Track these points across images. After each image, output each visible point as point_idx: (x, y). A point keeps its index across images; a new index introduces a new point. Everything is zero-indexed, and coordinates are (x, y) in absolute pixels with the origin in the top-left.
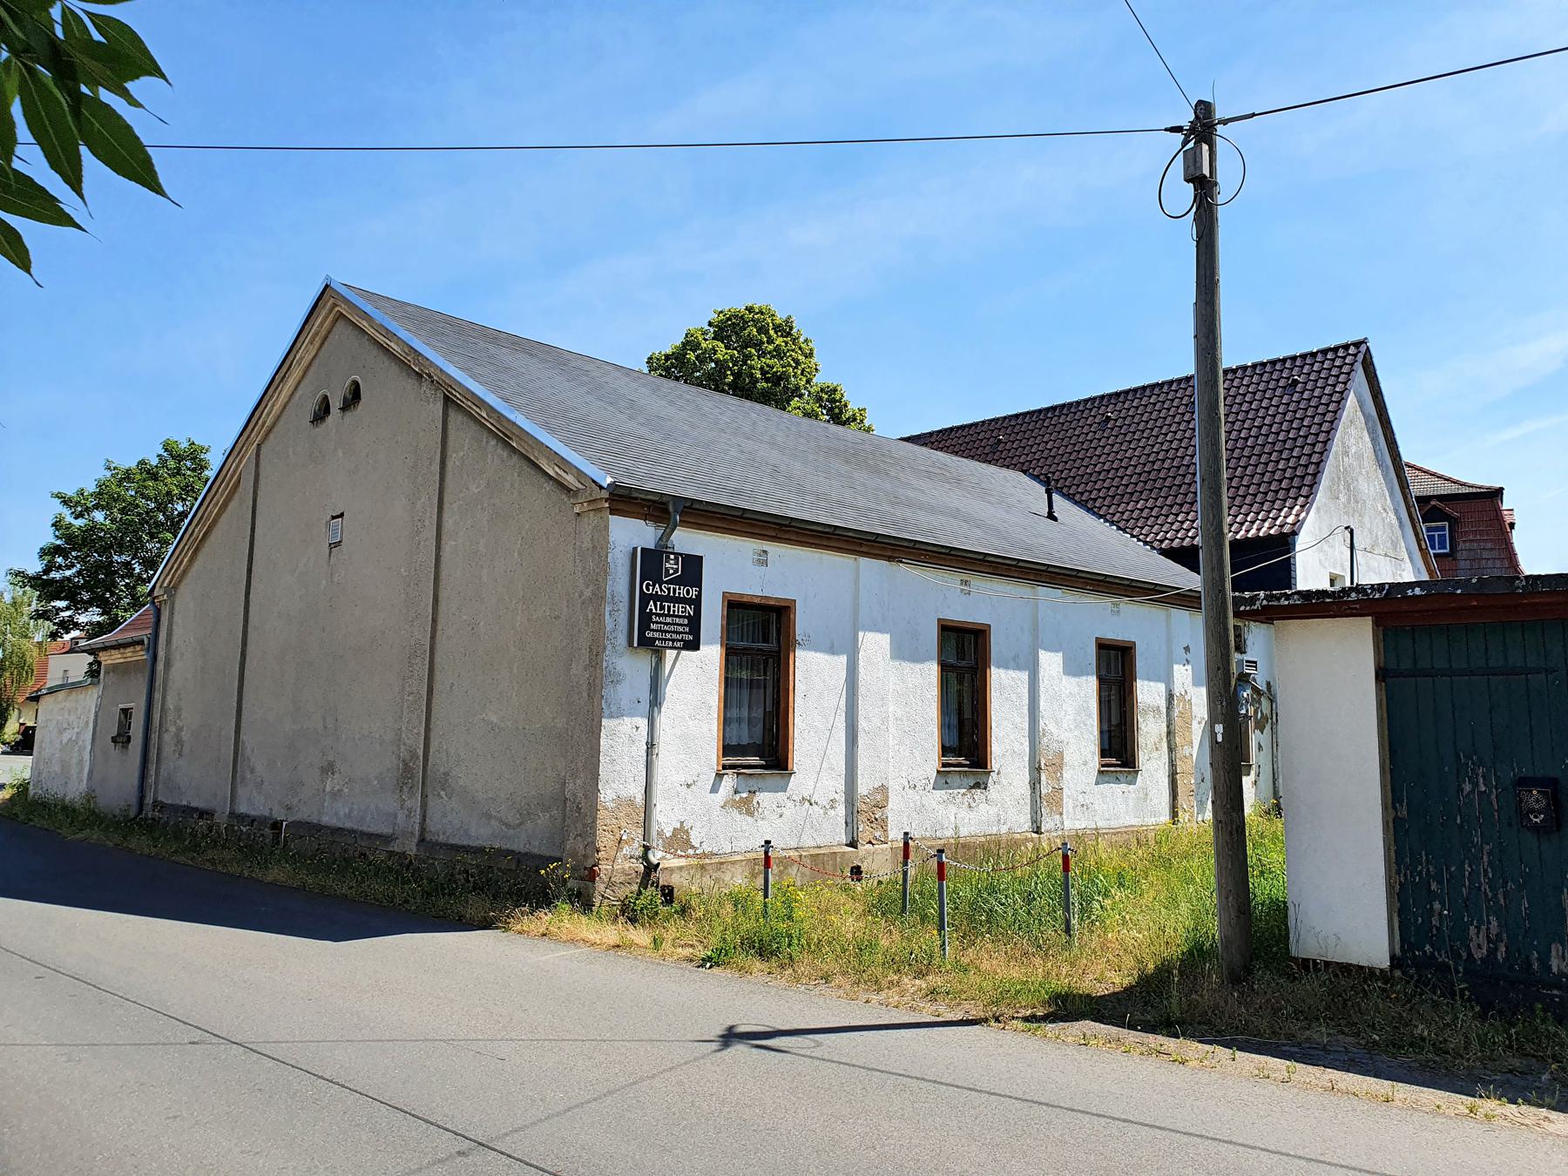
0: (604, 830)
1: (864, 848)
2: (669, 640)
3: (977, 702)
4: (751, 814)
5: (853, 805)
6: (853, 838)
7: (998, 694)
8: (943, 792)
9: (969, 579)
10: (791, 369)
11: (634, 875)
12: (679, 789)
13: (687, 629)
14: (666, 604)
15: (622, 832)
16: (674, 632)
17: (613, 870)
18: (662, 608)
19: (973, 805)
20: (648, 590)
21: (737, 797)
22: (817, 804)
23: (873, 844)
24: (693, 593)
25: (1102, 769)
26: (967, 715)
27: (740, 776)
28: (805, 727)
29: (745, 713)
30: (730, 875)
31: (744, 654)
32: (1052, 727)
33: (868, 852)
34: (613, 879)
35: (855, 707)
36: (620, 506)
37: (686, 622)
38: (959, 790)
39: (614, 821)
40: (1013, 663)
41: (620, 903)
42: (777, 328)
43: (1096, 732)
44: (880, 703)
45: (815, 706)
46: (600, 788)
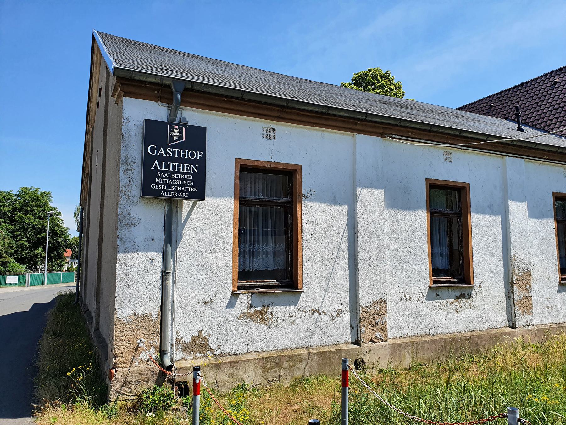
0: (121, 340)
1: (365, 346)
2: (174, 191)
3: (462, 237)
4: (266, 323)
5: (357, 313)
6: (357, 337)
7: (478, 232)
8: (435, 302)
9: (450, 151)
10: (388, 93)
11: (150, 374)
12: (198, 306)
13: (192, 183)
14: (171, 164)
15: (139, 341)
16: (179, 185)
17: (129, 372)
18: (167, 166)
19: (460, 310)
20: (153, 152)
21: (252, 310)
22: (325, 313)
23: (374, 342)
24: (198, 155)
25: (562, 281)
26: (456, 247)
27: (254, 295)
28: (313, 257)
29: (270, 248)
30: (244, 371)
31: (261, 205)
32: (521, 254)
33: (370, 349)
34: (128, 379)
35: (356, 242)
36: (130, 89)
37: (191, 177)
38: (447, 300)
39: (131, 333)
40: (490, 210)
41: (136, 397)
42: (382, 77)
43: (556, 256)
44: (377, 239)
45: (321, 241)
46: (116, 306)
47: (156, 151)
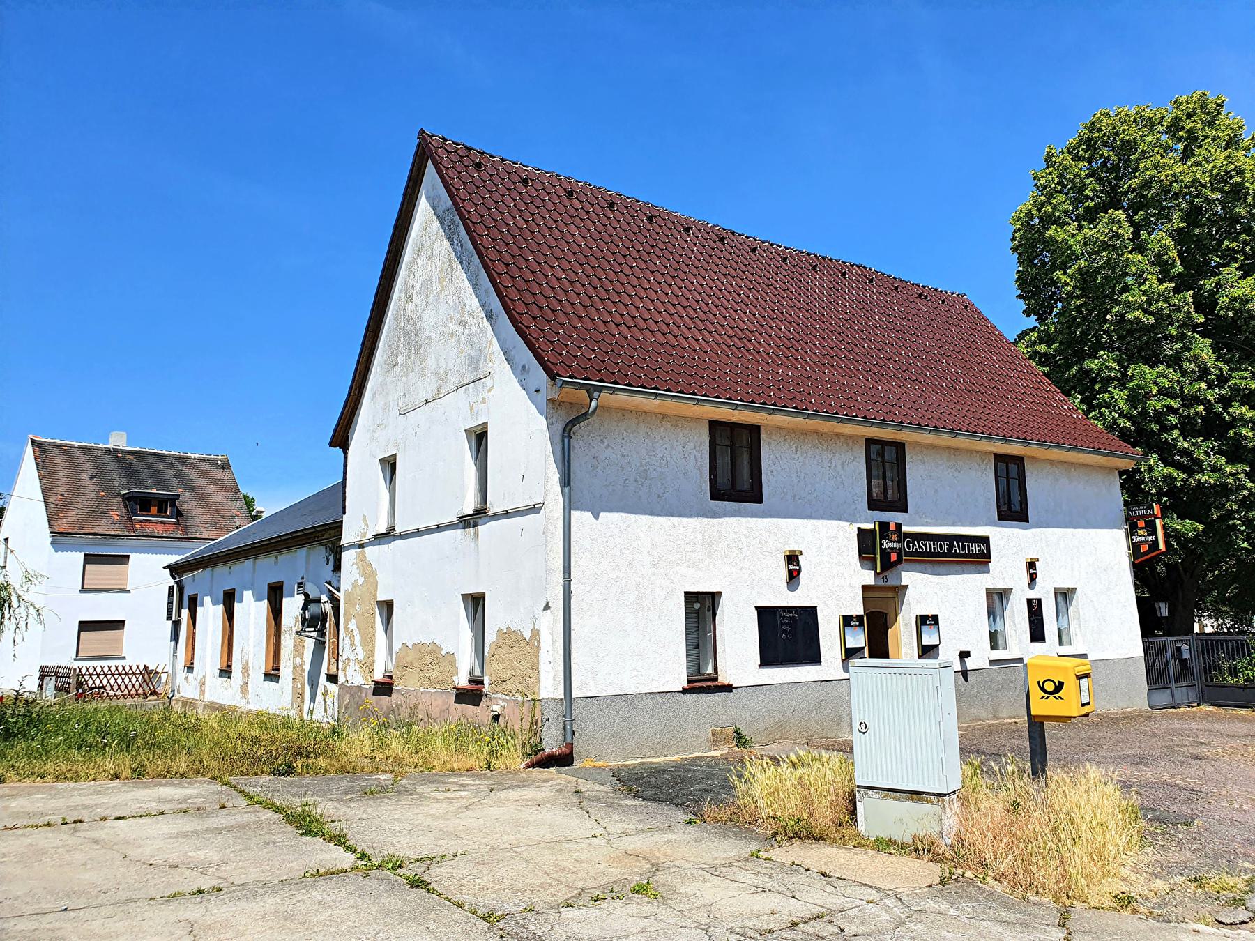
18: (964, 548)
20: (909, 548)
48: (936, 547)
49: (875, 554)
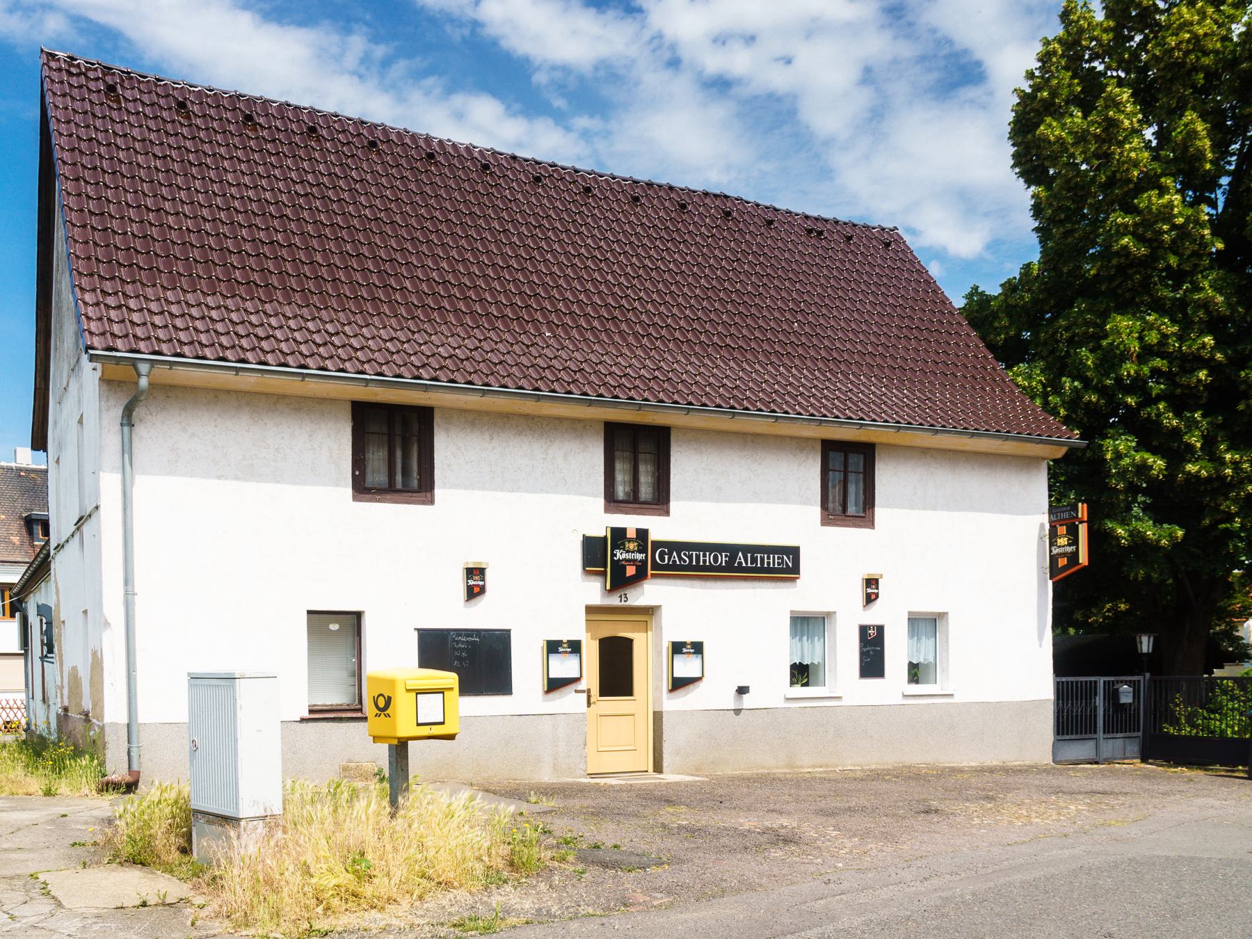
20: (662, 559)
47: (666, 557)
48: (709, 559)
49: (605, 567)
